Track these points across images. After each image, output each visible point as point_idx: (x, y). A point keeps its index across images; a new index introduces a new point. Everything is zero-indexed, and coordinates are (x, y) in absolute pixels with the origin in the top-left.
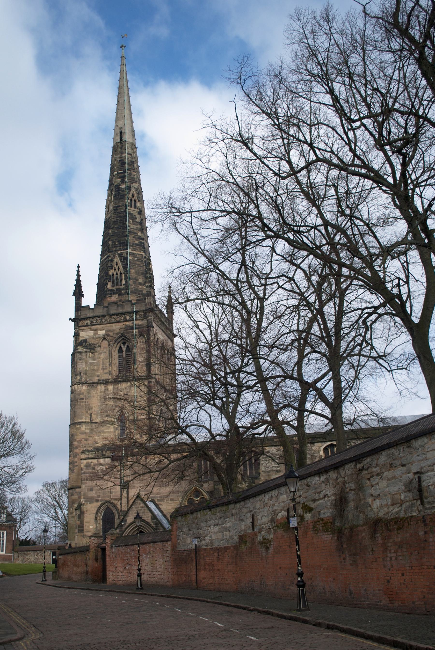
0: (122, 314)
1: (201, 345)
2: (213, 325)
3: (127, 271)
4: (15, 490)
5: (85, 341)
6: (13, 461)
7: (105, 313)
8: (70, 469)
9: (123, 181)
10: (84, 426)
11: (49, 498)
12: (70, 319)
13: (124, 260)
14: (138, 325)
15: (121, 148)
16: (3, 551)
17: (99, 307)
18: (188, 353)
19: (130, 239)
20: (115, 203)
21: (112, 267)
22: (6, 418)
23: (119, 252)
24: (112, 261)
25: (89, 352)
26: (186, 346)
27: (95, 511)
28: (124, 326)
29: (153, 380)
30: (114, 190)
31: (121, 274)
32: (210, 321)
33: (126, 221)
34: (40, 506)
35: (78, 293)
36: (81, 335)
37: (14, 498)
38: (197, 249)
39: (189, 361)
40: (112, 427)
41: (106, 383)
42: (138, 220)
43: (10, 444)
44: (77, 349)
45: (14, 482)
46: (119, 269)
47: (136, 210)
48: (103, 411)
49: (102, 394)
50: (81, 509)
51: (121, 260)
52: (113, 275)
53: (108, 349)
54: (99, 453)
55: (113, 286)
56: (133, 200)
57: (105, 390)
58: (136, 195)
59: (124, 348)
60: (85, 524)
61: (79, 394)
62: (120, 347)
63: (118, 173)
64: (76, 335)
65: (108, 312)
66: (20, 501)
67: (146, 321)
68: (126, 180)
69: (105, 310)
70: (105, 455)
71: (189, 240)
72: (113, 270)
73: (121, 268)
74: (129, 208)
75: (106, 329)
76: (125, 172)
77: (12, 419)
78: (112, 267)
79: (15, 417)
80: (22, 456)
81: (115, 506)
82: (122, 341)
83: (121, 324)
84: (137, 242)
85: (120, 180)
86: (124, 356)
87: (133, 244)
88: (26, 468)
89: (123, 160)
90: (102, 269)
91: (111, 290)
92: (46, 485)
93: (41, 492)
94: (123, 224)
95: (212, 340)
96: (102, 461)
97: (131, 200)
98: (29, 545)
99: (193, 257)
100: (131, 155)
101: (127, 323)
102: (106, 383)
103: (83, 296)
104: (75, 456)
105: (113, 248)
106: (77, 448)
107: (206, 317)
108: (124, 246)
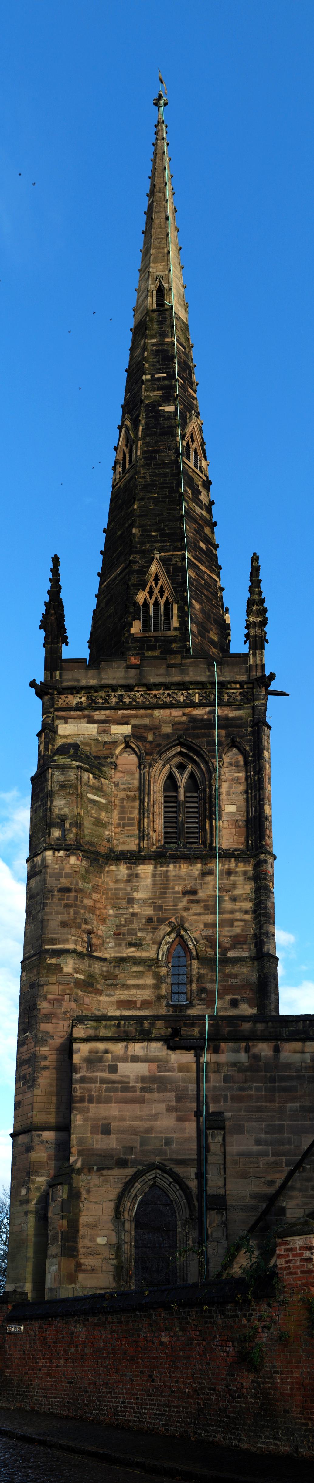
0: (183, 686)
5: (75, 746)
7: (132, 682)
9: (168, 398)
10: (71, 961)
12: (33, 684)
14: (227, 718)
15: (161, 323)
25: (87, 770)
27: (113, 1194)
28: (184, 718)
31: (167, 603)
36: (61, 731)
44: (55, 761)
46: (162, 592)
49: (121, 885)
50: (70, 1185)
53: (137, 776)
55: (144, 629)
57: (130, 875)
59: (182, 780)
60: (82, 1231)
61: (58, 876)
62: (171, 777)
64: (47, 731)
65: (140, 679)
67: (249, 711)
69: (133, 672)
70: (149, 1032)
75: (134, 721)
76: (171, 377)
81: (179, 1180)
82: (176, 760)
83: (177, 713)
86: (182, 798)
89: (167, 351)
96: (137, 1048)
98: (125, 1120)
101: (196, 712)
105: (143, 543)
106: (48, 1018)
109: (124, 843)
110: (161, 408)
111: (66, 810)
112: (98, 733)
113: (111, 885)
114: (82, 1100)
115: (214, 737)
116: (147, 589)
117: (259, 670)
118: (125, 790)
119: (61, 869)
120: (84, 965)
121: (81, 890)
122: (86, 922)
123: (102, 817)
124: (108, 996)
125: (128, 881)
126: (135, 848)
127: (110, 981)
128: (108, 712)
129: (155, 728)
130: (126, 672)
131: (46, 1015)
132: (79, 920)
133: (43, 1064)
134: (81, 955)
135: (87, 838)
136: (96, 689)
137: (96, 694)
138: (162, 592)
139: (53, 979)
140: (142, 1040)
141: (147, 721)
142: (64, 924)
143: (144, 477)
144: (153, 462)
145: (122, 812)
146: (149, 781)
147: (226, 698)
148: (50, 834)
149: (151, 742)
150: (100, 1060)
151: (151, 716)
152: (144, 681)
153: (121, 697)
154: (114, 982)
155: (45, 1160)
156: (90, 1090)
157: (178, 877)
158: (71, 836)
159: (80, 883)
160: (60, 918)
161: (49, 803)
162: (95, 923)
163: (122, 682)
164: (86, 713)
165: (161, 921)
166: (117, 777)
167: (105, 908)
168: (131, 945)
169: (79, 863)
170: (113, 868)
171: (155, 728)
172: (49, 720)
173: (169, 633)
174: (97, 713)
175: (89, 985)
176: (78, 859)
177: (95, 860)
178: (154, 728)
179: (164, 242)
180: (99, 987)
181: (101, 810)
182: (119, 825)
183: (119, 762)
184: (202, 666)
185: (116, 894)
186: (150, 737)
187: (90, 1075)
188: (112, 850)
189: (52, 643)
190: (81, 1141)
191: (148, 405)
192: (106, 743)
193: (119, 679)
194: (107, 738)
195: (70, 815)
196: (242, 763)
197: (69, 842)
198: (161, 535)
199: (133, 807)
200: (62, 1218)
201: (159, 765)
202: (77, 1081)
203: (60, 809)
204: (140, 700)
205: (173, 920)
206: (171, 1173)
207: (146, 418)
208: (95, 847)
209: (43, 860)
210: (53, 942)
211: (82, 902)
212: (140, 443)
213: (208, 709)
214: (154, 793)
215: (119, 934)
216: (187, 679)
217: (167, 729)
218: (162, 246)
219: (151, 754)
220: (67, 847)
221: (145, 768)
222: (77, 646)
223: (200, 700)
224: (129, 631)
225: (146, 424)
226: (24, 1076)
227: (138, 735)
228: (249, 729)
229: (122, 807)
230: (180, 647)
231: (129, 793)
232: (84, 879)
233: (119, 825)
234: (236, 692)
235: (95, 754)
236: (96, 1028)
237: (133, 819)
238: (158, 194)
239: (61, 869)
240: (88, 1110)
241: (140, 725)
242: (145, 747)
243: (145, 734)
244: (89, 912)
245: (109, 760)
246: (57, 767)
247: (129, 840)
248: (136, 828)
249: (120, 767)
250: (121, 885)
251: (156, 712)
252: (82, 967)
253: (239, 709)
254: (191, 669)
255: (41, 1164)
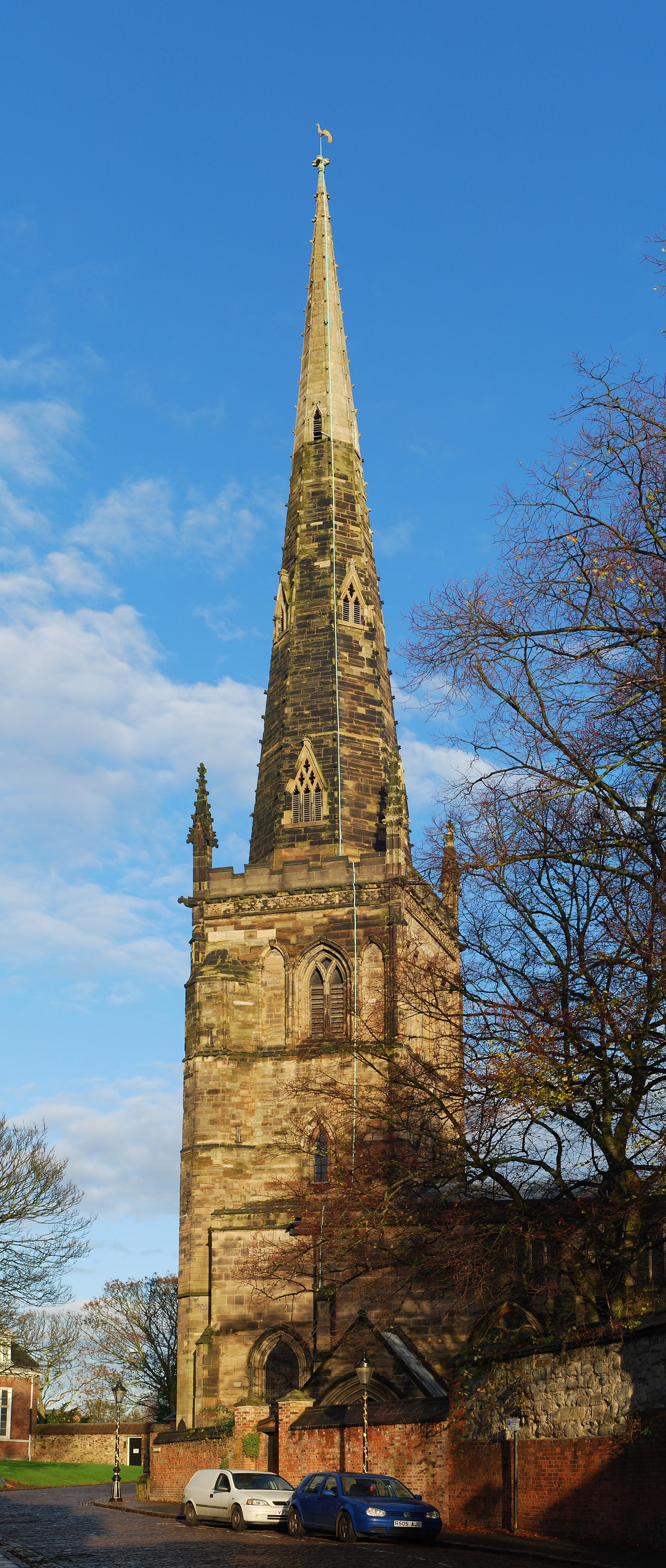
0: (322, 889)
1: (543, 971)
2: (574, 923)
3: (334, 785)
4: (40, 1295)
5: (223, 953)
6: (32, 1230)
7: (275, 887)
8: (182, 1251)
9: (323, 551)
11: (122, 1318)
12: (181, 900)
13: (326, 755)
14: (365, 918)
15: (318, 458)
16: (3, 1433)
17: (259, 871)
18: (503, 990)
19: (342, 702)
20: (301, 609)
21: (292, 773)
22: (16, 1131)
23: (313, 735)
24: (294, 757)
25: (232, 980)
26: (498, 971)
28: (325, 920)
29: (403, 1052)
30: (297, 573)
31: (318, 790)
32: (567, 910)
33: (332, 655)
34: (99, 1335)
35: (203, 838)
37: (30, 1315)
38: (540, 729)
39: (506, 1006)
40: (293, 1158)
41: (278, 1054)
42: (366, 653)
43: (27, 1191)
44: (202, 973)
45: (36, 1279)
46: (312, 778)
47: (360, 626)
48: (271, 1120)
49: (268, 1080)
51: (317, 755)
52: (297, 792)
54: (259, 1219)
56: (352, 600)
58: (358, 588)
59: (328, 974)
61: (207, 1080)
63: (309, 529)
64: (198, 939)
65: (282, 885)
66: (48, 1323)
67: (387, 910)
68: (333, 546)
69: (276, 878)
70: (274, 1222)
71: (516, 707)
72: (297, 781)
73: (319, 778)
74: (341, 622)
75: (278, 925)
76: (328, 525)
77: (31, 1133)
78: (292, 773)
79: (40, 1128)
80: (57, 1220)
82: (324, 955)
83: (318, 915)
84: (362, 710)
85: (315, 545)
87: (351, 715)
88: (70, 1246)
89: (323, 492)
90: (267, 778)
91: (291, 831)
92: (114, 1287)
93: (102, 1303)
94: (324, 663)
95: (569, 958)
96: (268, 1235)
97: (346, 600)
99: (525, 751)
100: (345, 477)
102: (278, 1054)
103: (215, 844)
104: (196, 1223)
105: (295, 723)
106: (201, 1203)
107: (555, 900)
108: (325, 719)
109: (272, 1039)
110: (316, 564)
111: (213, 1020)
112: (245, 938)
113: (259, 1080)
114: (220, 1278)
115: (352, 936)
116: (298, 776)
117: (395, 868)
118: (272, 989)
119: (210, 1073)
120: (233, 1155)
121: (229, 1090)
122: (234, 1117)
123: (248, 1019)
124: (257, 1179)
125: (274, 1076)
126: (282, 1043)
127: (258, 1166)
128: (254, 918)
129: (298, 931)
130: (269, 878)
131: (199, 1201)
132: (226, 1117)
133: (198, 1241)
134: (230, 1147)
135: (234, 1042)
136: (242, 897)
137: (242, 901)
138: (312, 778)
139: (206, 1170)
140: (269, 1229)
141: (290, 925)
142: (213, 1122)
143: (297, 648)
144: (307, 630)
145: (270, 1010)
146: (293, 982)
147: (365, 896)
148: (199, 1041)
149: (294, 945)
150: (234, 1246)
151: (294, 919)
152: (287, 886)
153: (265, 902)
154: (262, 1167)
155: (201, 1319)
156: (226, 1269)
157: (319, 1070)
158: (219, 1042)
159: (227, 1083)
160: (209, 1117)
161: (198, 1014)
162: (243, 1116)
163: (266, 888)
164: (233, 919)
165: (304, 1111)
166: (265, 977)
167: (253, 1101)
168: (276, 1133)
169: (226, 1066)
170: (260, 1064)
171: (298, 931)
172: (199, 930)
173: (319, 823)
174: (244, 918)
175: (239, 1172)
176: (225, 1063)
177: (242, 1060)
178: (297, 931)
179: (323, 353)
180: (248, 1172)
181: (248, 1012)
182: (267, 1022)
183: (266, 963)
184: (341, 868)
185: (263, 1088)
186: (293, 940)
187: (225, 1257)
188: (260, 1048)
189: (200, 854)
190: (219, 1310)
191: (303, 561)
192: (252, 948)
193: (263, 885)
194: (253, 943)
195: (216, 1023)
196: (381, 958)
197: (216, 1049)
198: (313, 714)
199: (279, 1005)
200: (204, 1369)
201: (304, 962)
202: (215, 1263)
203: (207, 1019)
204: (283, 903)
205: (314, 1109)
206: (292, 1333)
207: (301, 577)
208: (242, 1048)
209: (194, 1065)
210: (204, 1137)
211: (229, 1100)
212: (294, 608)
213: (347, 909)
214: (300, 990)
215: (266, 1124)
216: (327, 882)
217: (309, 931)
218: (320, 359)
219: (294, 956)
220: (215, 1054)
221: (289, 969)
222: (233, 848)
223: (340, 901)
224: (280, 822)
225: (301, 585)
226: (185, 1250)
227: (282, 939)
228: (387, 927)
229: (270, 1006)
230: (329, 837)
231: (276, 992)
232: (231, 1079)
233: (267, 1022)
234: (375, 892)
235: (242, 959)
236: (231, 1220)
237: (280, 1016)
238: (317, 291)
239: (210, 1073)
240: (225, 1285)
241: (284, 929)
242: (288, 949)
243: (288, 938)
244: (237, 1108)
245: (255, 964)
246: (204, 979)
247: (276, 1036)
248: (283, 1024)
249: (267, 968)
250: (268, 1080)
251: (300, 916)
252: (231, 1158)
253: (376, 908)
254: (330, 871)
255: (198, 1322)
